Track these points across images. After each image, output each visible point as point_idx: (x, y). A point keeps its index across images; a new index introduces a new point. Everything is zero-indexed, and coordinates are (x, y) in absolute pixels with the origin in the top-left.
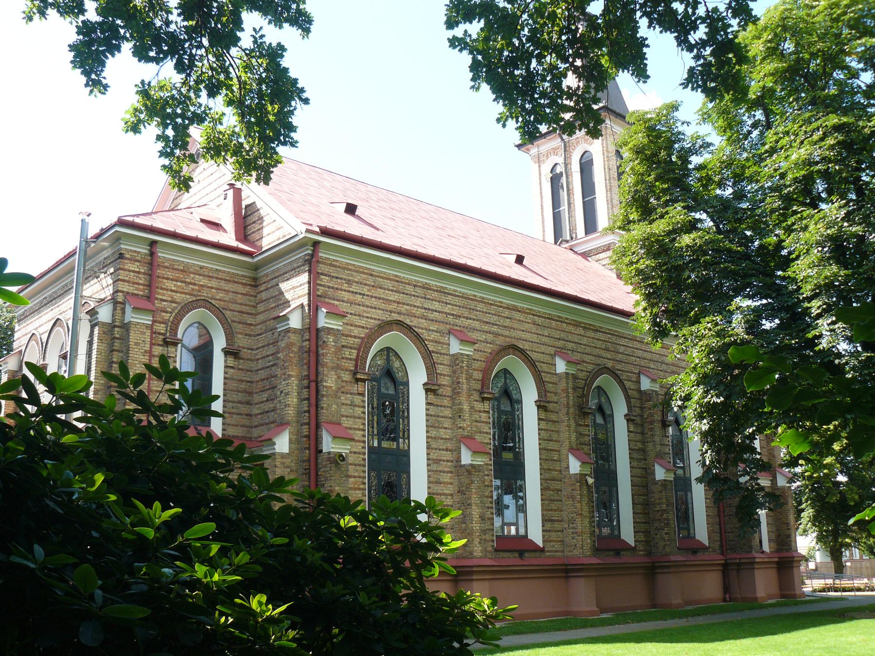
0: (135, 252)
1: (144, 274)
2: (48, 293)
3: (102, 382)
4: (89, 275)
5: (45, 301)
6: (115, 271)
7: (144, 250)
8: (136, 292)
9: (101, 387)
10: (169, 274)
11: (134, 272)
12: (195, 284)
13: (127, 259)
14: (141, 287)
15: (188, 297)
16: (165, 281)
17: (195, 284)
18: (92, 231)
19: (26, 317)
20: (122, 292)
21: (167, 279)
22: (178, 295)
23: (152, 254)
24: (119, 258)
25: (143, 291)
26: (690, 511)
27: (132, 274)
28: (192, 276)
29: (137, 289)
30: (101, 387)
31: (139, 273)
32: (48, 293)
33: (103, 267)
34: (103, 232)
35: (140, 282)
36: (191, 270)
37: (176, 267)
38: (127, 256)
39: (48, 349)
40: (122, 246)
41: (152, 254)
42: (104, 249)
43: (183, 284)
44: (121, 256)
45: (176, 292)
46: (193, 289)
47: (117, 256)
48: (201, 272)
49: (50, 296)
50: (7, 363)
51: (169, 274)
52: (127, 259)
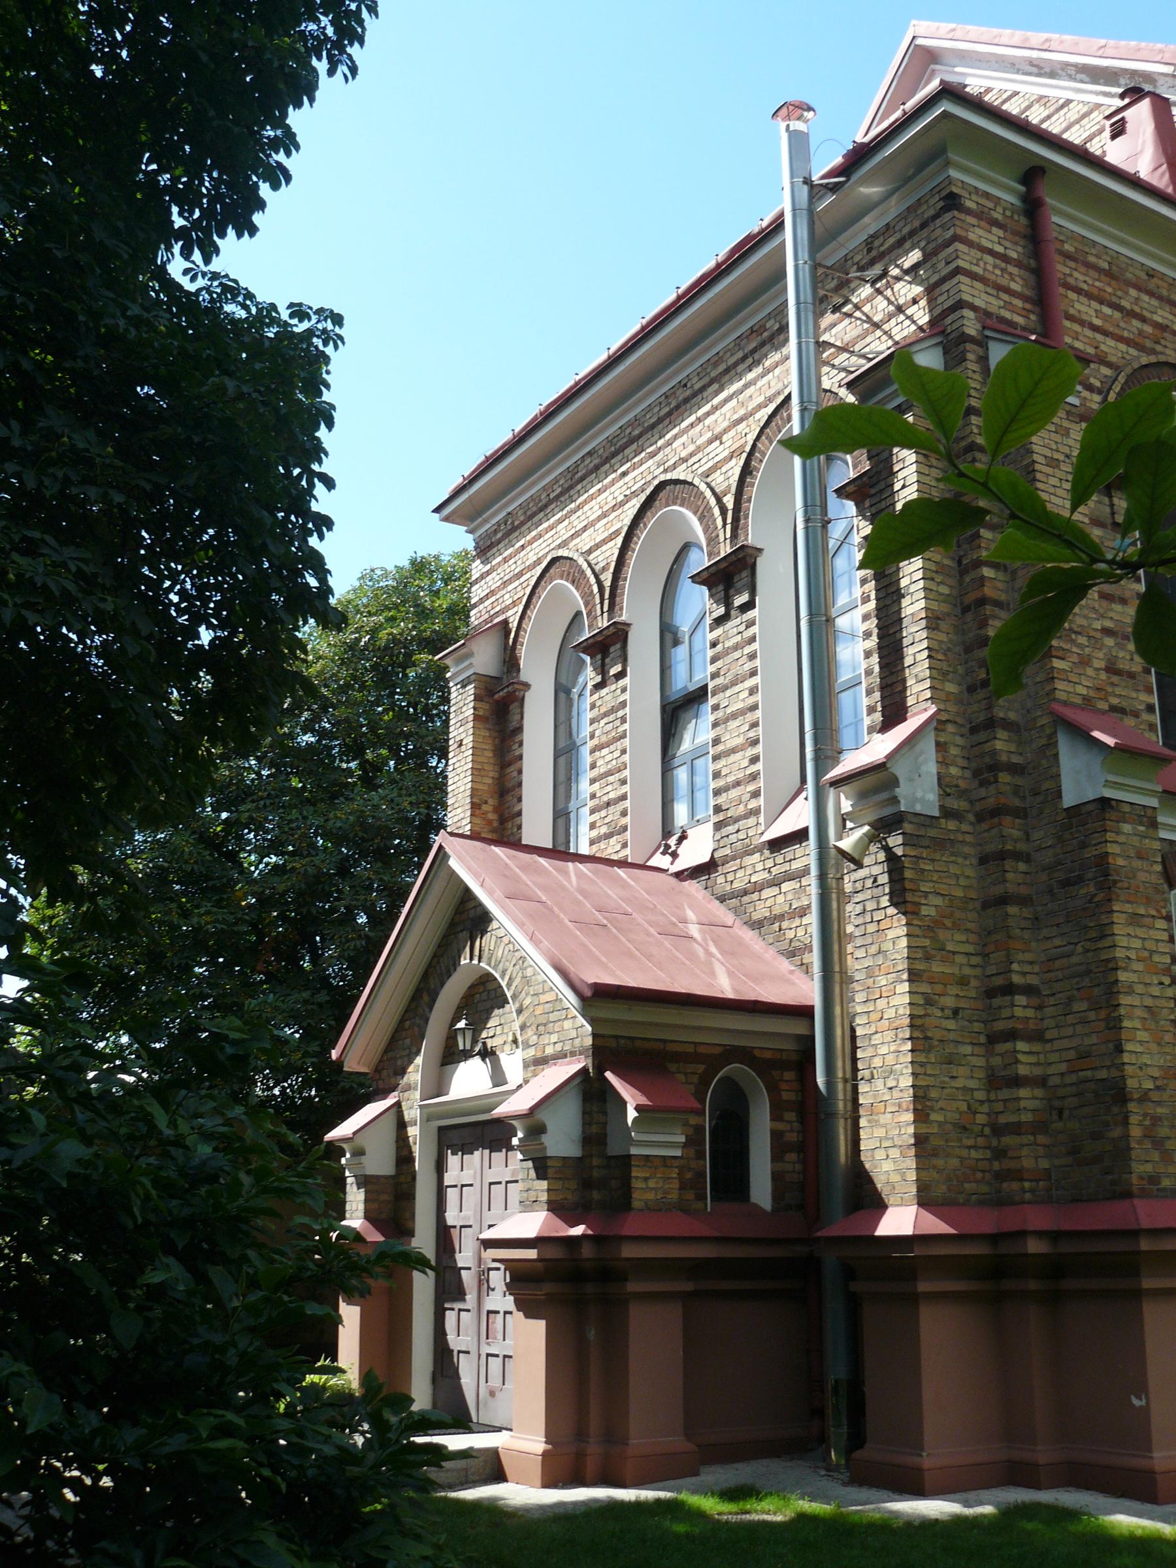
0: (987, 195)
1: (1018, 264)
2: (597, 440)
3: (944, 590)
4: (831, 289)
5: (590, 463)
6: (927, 257)
7: (1008, 195)
8: (1007, 315)
9: (945, 608)
10: (1079, 277)
11: (991, 252)
12: (1143, 320)
13: (969, 212)
14: (1019, 303)
15: (1133, 352)
16: (1072, 295)
17: (1143, 320)
18: (826, 160)
19: (514, 529)
20: (974, 308)
21: (1079, 291)
22: (1111, 343)
23: (1032, 207)
24: (946, 209)
25: (1025, 313)
26: (443, 1431)
27: (989, 259)
28: (1133, 292)
29: (1007, 306)
30: (945, 608)
31: (1004, 258)
32: (597, 440)
33: (872, 263)
34: (859, 156)
35: (1014, 286)
36: (1129, 275)
37: (1092, 259)
38: (969, 204)
39: (627, 586)
40: (953, 173)
41: (1032, 207)
42: (868, 207)
43: (1117, 315)
44: (952, 202)
45: (1106, 333)
46: (1141, 333)
47: (936, 203)
48: (1152, 284)
49: (610, 441)
50: (470, 655)
51: (1079, 277)
52: (969, 212)
